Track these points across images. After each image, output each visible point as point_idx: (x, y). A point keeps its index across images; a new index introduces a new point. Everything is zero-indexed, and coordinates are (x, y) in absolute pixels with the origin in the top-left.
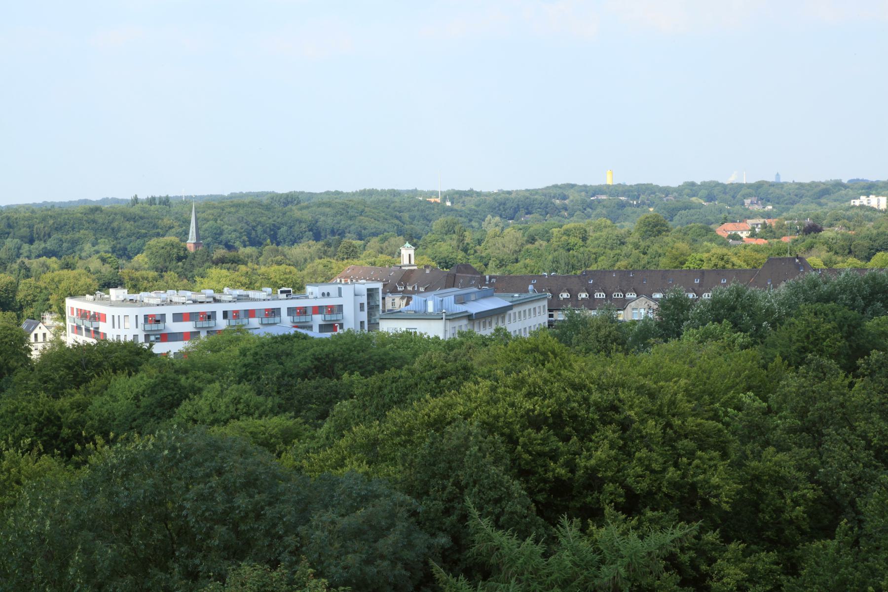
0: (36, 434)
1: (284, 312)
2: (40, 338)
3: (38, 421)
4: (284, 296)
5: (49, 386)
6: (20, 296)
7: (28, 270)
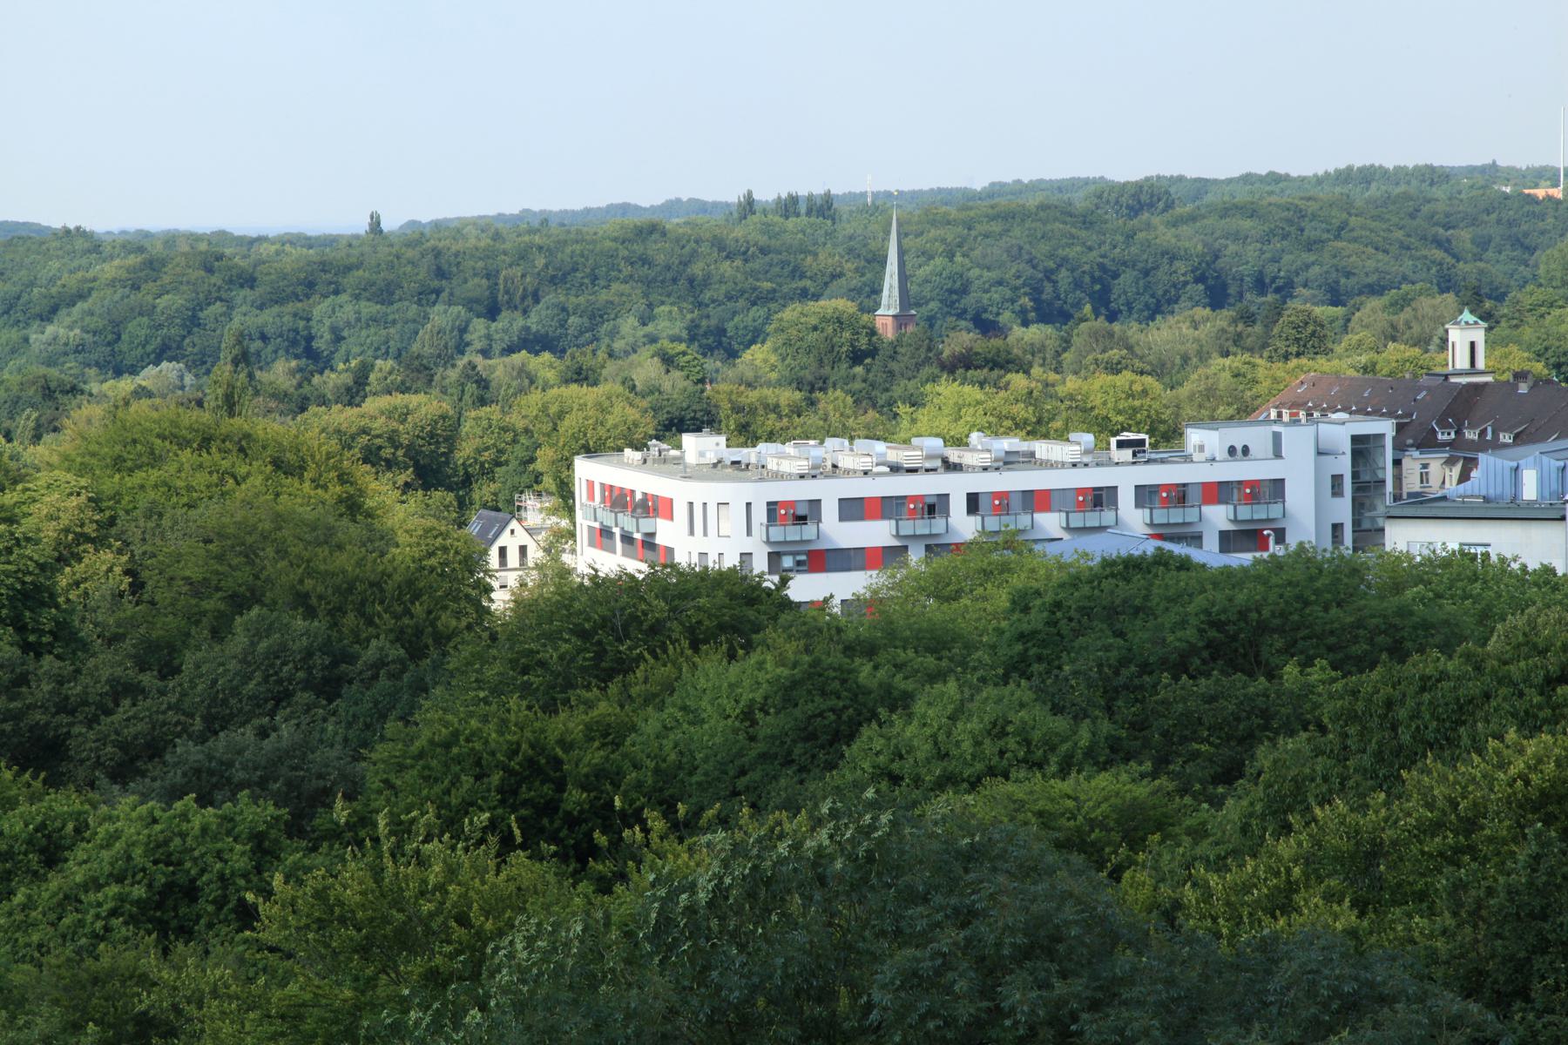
0: (503, 802)
1: (1126, 498)
2: (513, 559)
3: (505, 769)
4: (1127, 454)
5: (534, 679)
6: (464, 451)
7: (483, 383)
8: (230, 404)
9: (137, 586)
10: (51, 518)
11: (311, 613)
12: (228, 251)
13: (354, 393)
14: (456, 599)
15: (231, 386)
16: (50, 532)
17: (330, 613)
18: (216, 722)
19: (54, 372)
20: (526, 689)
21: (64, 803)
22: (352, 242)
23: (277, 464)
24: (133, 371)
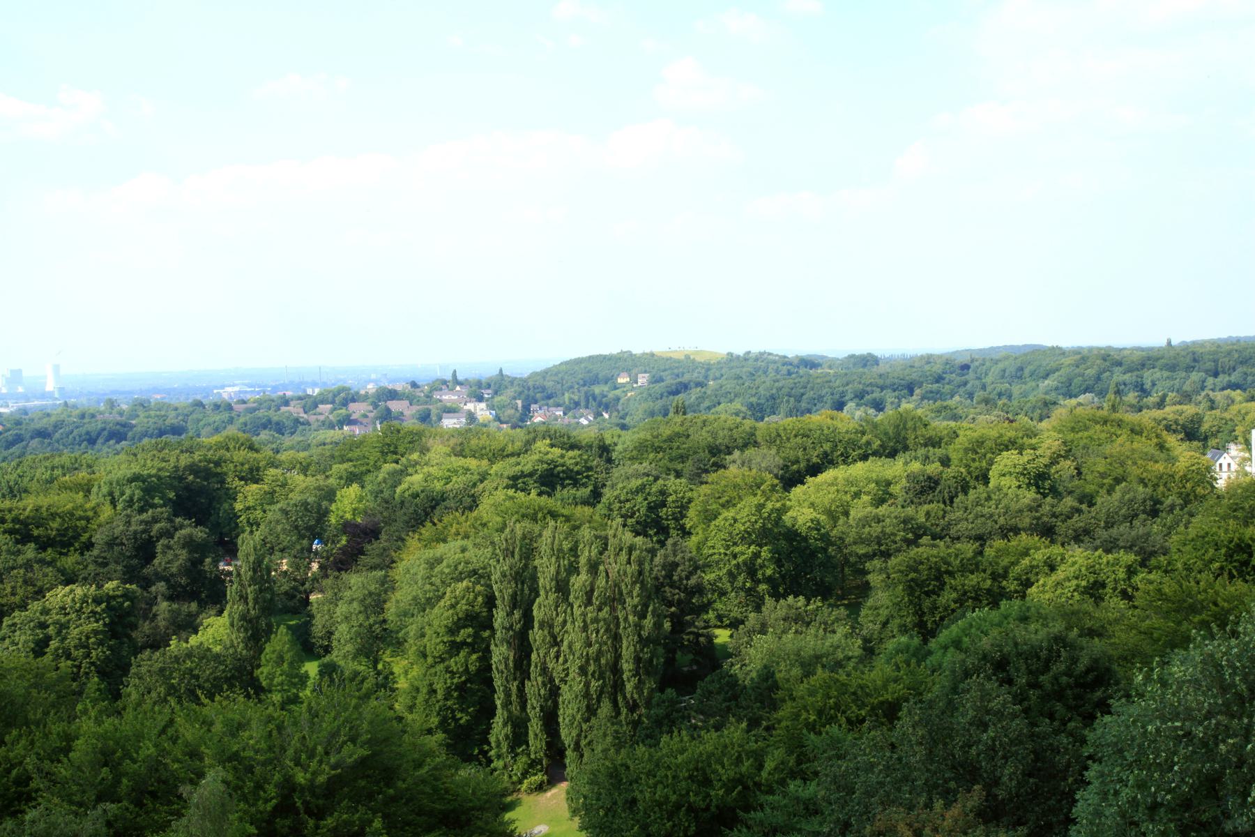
0: (1226, 560)
3: (1228, 547)
5: (1239, 514)
6: (1205, 427)
7: (1212, 401)
8: (1114, 408)
9: (1079, 473)
10: (1048, 448)
11: (1146, 486)
12: (1112, 353)
13: (1161, 404)
14: (1203, 483)
15: (1114, 401)
16: (1048, 453)
17: (1153, 486)
18: (1109, 525)
19: (1048, 397)
20: (1236, 518)
21: (1056, 550)
22: (1159, 349)
23: (1132, 431)
24: (1076, 396)
